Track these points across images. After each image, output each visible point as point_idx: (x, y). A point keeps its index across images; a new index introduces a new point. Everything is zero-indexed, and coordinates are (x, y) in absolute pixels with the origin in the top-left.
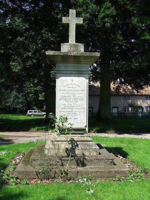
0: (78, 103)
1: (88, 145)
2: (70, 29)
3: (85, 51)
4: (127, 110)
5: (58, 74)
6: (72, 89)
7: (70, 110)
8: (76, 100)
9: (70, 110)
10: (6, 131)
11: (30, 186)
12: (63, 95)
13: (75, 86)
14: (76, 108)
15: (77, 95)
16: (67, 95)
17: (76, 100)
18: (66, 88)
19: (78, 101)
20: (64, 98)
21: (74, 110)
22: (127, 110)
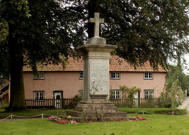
0: (103, 79)
1: (110, 106)
2: (96, 27)
3: (107, 43)
4: (116, 95)
5: (91, 59)
6: (99, 69)
7: (98, 83)
8: (102, 76)
9: (98, 83)
10: (94, 27)
11: (155, 127)
12: (94, 73)
13: (101, 67)
14: (102, 81)
15: (102, 73)
16: (96, 73)
17: (102, 76)
18: (95, 69)
19: (103, 77)
20: (94, 75)
21: (100, 83)
22: (116, 95)
